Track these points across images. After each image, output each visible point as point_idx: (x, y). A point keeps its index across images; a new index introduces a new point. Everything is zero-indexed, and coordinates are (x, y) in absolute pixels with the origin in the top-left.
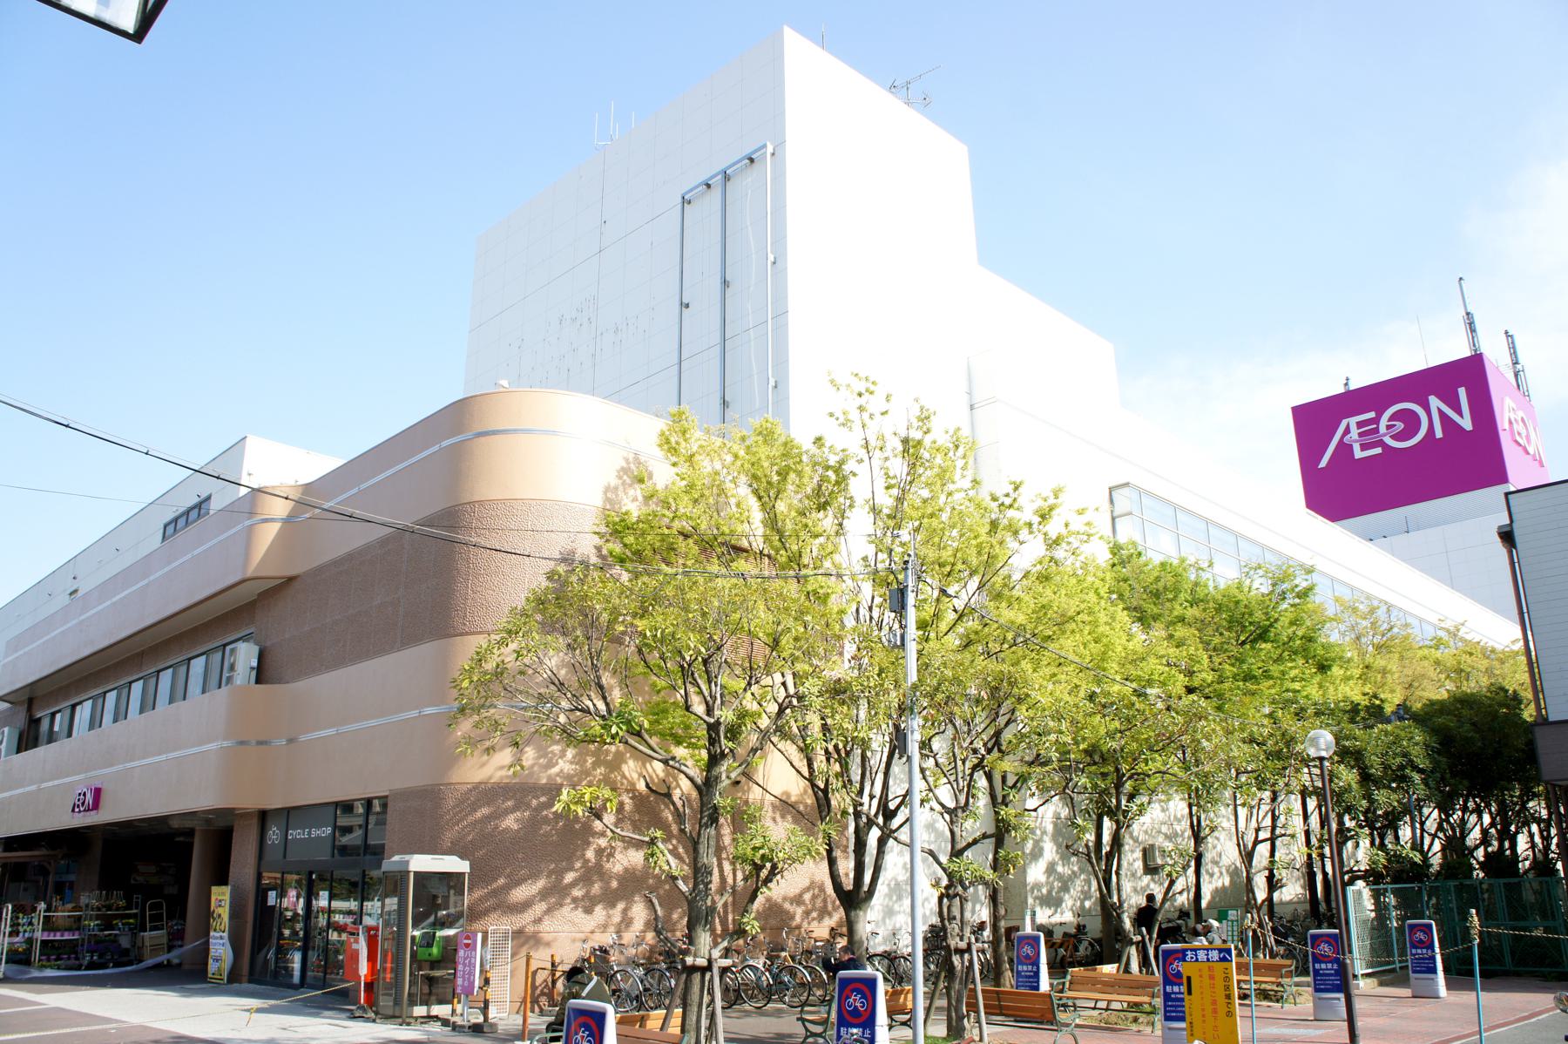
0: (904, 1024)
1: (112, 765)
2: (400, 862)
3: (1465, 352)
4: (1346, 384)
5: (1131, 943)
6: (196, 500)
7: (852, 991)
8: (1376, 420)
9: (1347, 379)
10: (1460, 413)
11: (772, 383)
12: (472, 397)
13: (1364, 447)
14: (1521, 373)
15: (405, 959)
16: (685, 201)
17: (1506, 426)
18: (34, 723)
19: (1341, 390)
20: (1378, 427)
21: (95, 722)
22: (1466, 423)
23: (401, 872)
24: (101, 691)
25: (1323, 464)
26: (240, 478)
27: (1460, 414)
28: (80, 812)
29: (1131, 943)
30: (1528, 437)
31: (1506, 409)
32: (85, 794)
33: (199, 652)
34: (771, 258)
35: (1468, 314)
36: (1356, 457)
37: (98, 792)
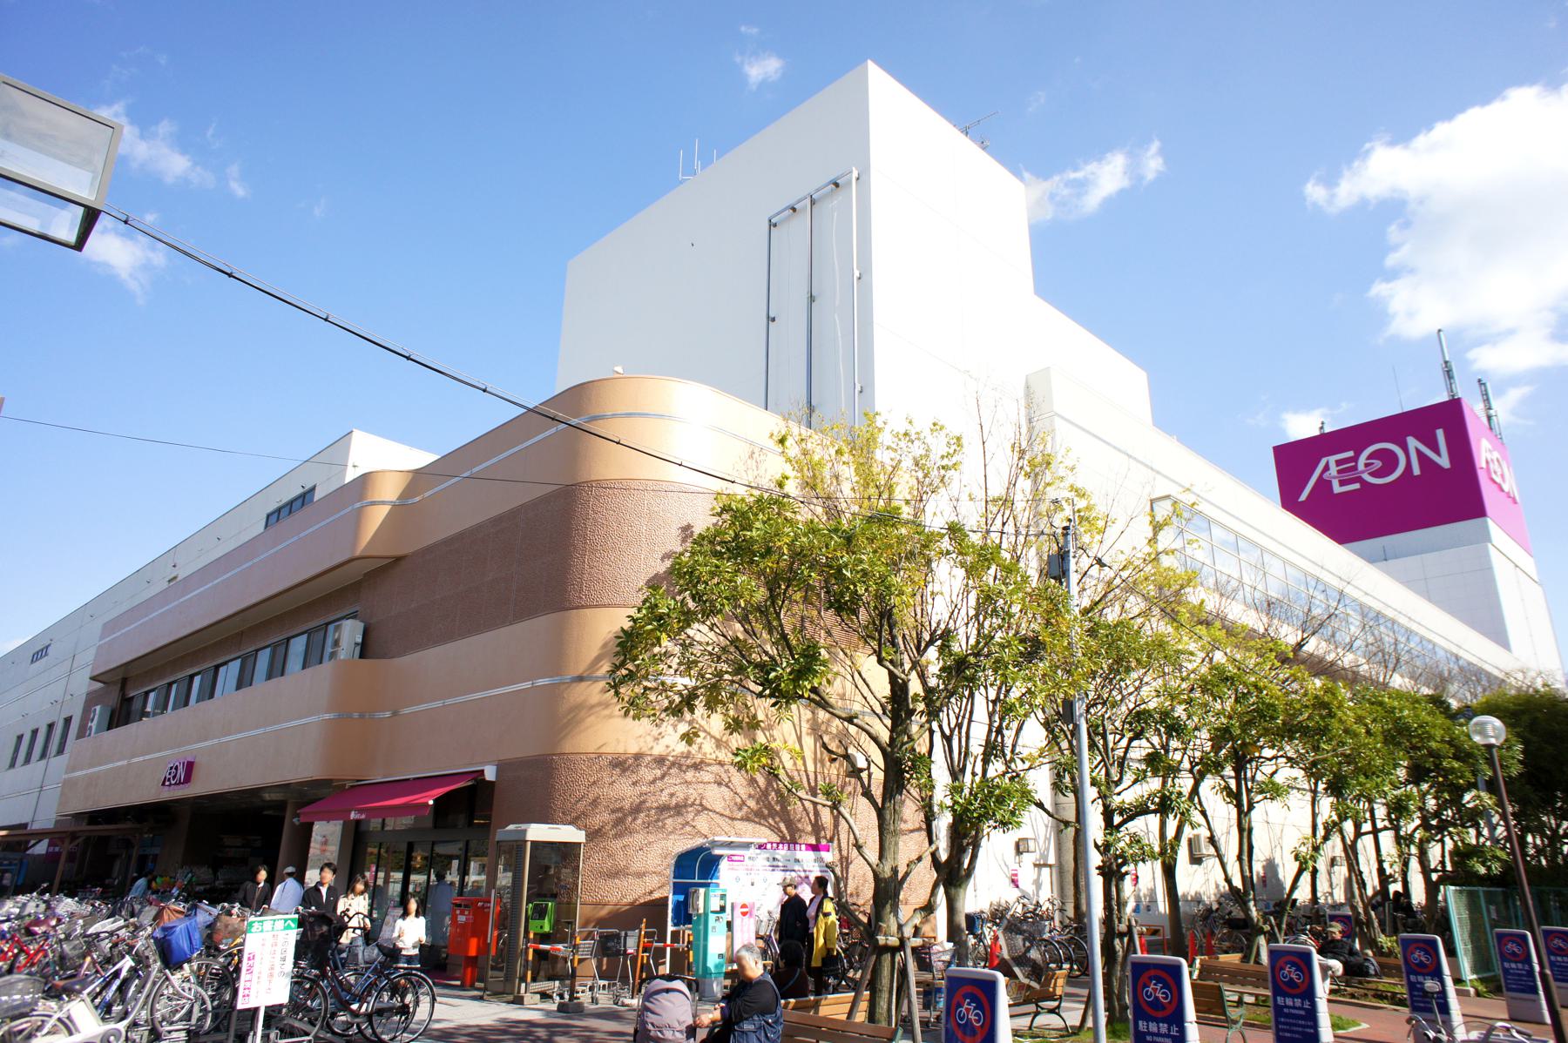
0: (1052, 1011)
1: (206, 740)
2: (516, 831)
3: (1443, 397)
4: (1321, 428)
5: (1261, 931)
6: (301, 491)
7: (1151, 979)
8: (1355, 459)
9: (1323, 423)
10: (1437, 451)
11: (858, 388)
12: (584, 383)
13: (1342, 483)
14: (1494, 418)
15: (519, 932)
16: (772, 225)
17: (1484, 465)
18: (126, 701)
19: (1316, 433)
21: (243, 682)
22: (1444, 461)
23: (516, 841)
24: (321, 621)
25: (1303, 497)
27: (1437, 452)
28: (170, 785)
29: (1261, 931)
30: (1502, 476)
31: (1484, 451)
32: (176, 768)
33: (299, 631)
34: (857, 274)
35: (1446, 362)
37: (190, 767)
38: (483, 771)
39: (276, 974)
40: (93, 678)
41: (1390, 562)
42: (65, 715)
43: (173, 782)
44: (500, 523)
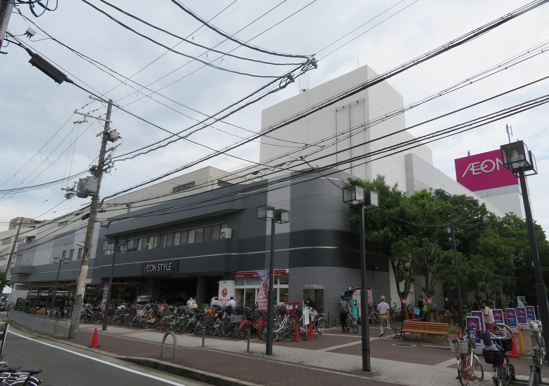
8: (480, 164)
13: (476, 172)
16: (337, 111)
19: (467, 155)
25: (463, 176)
26: (6, 314)
38: (286, 270)
40: (105, 236)
41: (490, 198)
44: (106, 147)
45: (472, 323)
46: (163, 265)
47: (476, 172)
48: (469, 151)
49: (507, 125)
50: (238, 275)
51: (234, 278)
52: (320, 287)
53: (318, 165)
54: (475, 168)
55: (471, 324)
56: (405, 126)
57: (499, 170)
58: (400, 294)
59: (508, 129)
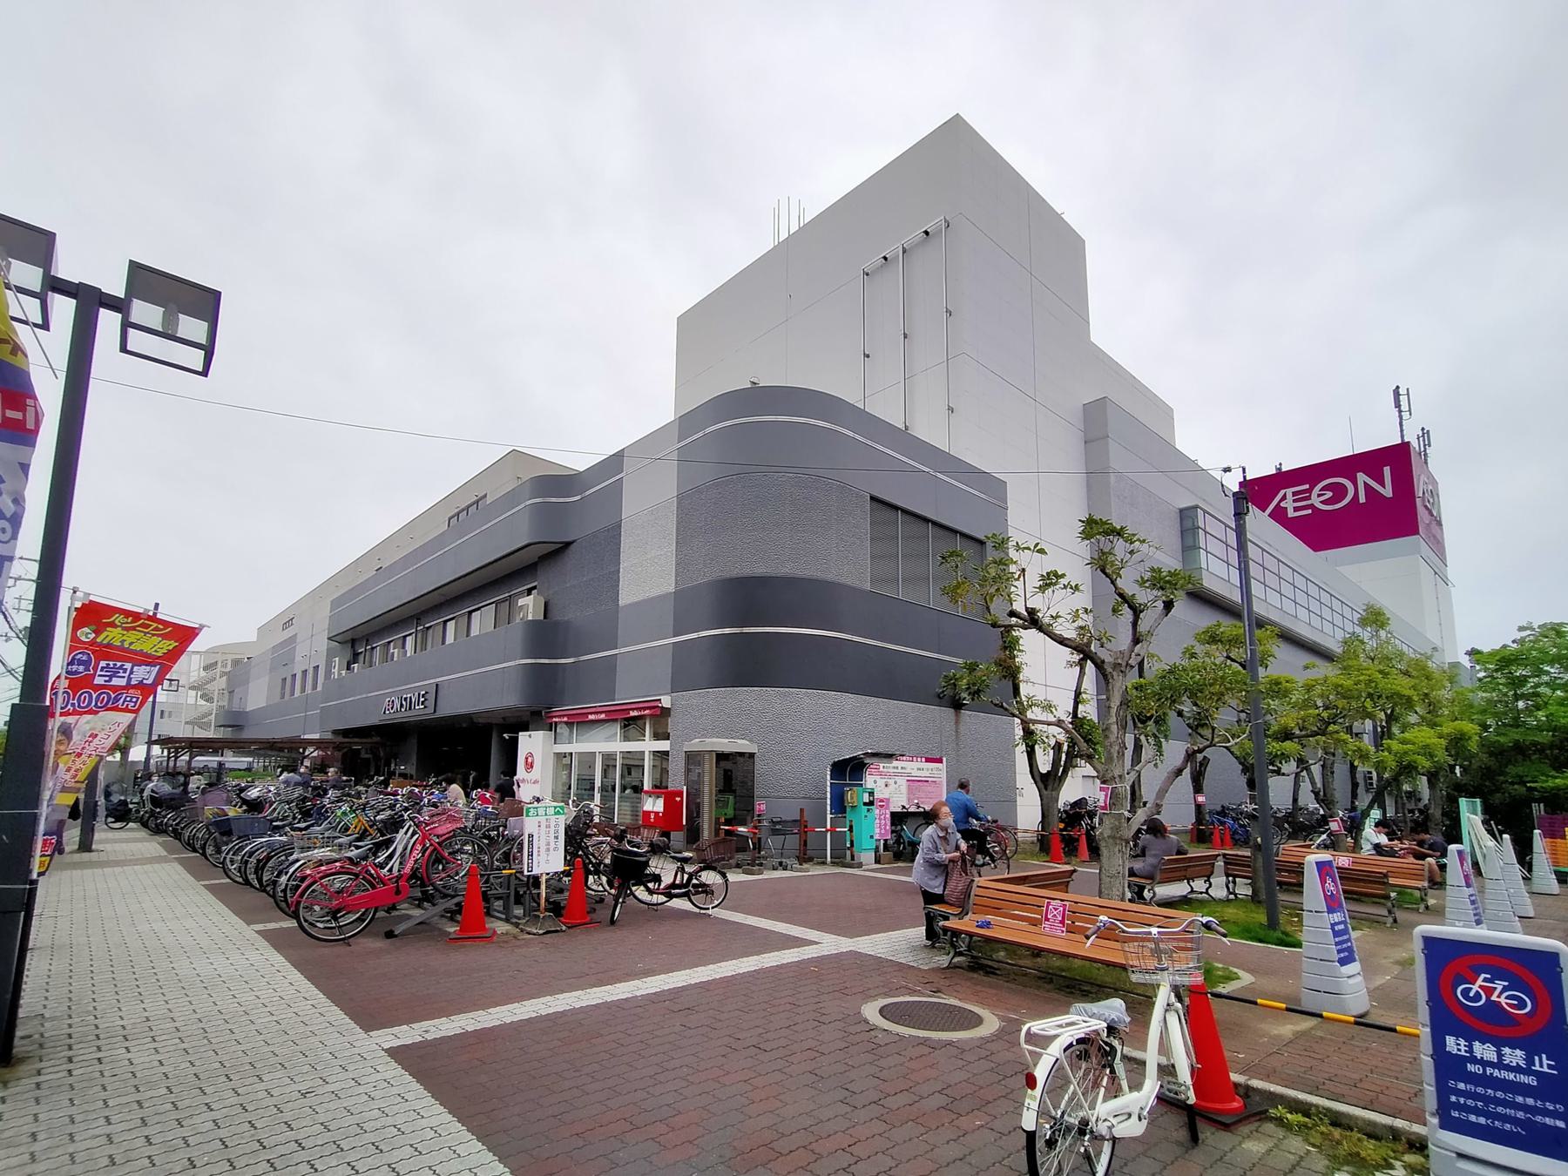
8: (1310, 491)
13: (1296, 509)
20: (1310, 496)
22: (1387, 491)
36: (1289, 516)
39: (551, 849)
42: (312, 665)
43: (392, 711)
45: (1480, 982)
46: (411, 698)
47: (1296, 509)
48: (1280, 464)
49: (1398, 387)
50: (555, 717)
51: (551, 724)
52: (742, 745)
53: (756, 381)
54: (1294, 501)
55: (1475, 988)
56: (1088, 323)
57: (1385, 468)
58: (1038, 779)
59: (1399, 398)
